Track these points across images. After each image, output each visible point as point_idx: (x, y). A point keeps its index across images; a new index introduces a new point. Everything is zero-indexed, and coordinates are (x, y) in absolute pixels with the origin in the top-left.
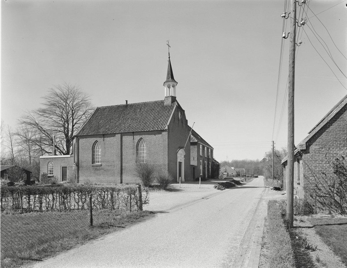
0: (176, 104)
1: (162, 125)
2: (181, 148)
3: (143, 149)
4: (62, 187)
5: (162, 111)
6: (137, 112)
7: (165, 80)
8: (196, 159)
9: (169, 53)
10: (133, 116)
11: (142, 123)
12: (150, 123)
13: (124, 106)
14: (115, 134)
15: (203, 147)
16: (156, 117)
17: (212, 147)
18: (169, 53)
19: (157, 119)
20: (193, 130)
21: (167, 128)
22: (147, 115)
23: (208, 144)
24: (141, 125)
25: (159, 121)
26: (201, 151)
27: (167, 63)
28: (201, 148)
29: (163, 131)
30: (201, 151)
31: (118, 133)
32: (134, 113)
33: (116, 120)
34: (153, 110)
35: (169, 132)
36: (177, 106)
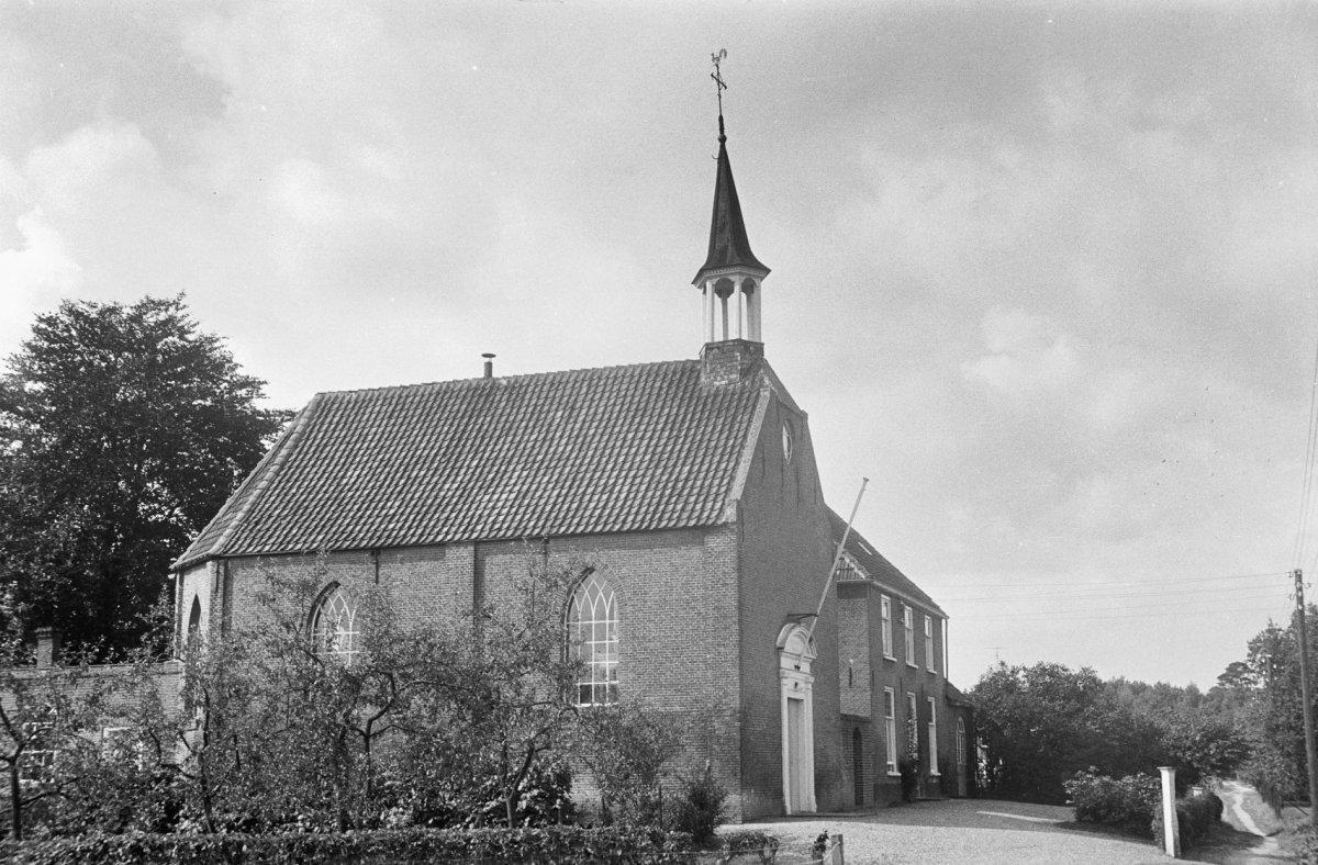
0: (767, 382)
1: (705, 501)
2: (794, 619)
3: (601, 628)
4: (1148, 694)
5: (691, 421)
6: (550, 425)
7: (702, 258)
8: (863, 679)
9: (721, 119)
10: (533, 447)
11: (588, 486)
12: (632, 484)
13: (476, 389)
14: (442, 544)
15: (898, 612)
16: (662, 453)
17: (937, 607)
18: (721, 119)
19: (671, 463)
20: (853, 533)
21: (730, 513)
22: (611, 444)
23: (919, 595)
24: (587, 498)
25: (683, 476)
26: (886, 630)
27: (713, 168)
28: (885, 612)
29: (703, 530)
30: (886, 630)
31: (459, 543)
32: (534, 427)
33: (437, 469)
34: (643, 416)
35: (741, 536)
36: (772, 392)
